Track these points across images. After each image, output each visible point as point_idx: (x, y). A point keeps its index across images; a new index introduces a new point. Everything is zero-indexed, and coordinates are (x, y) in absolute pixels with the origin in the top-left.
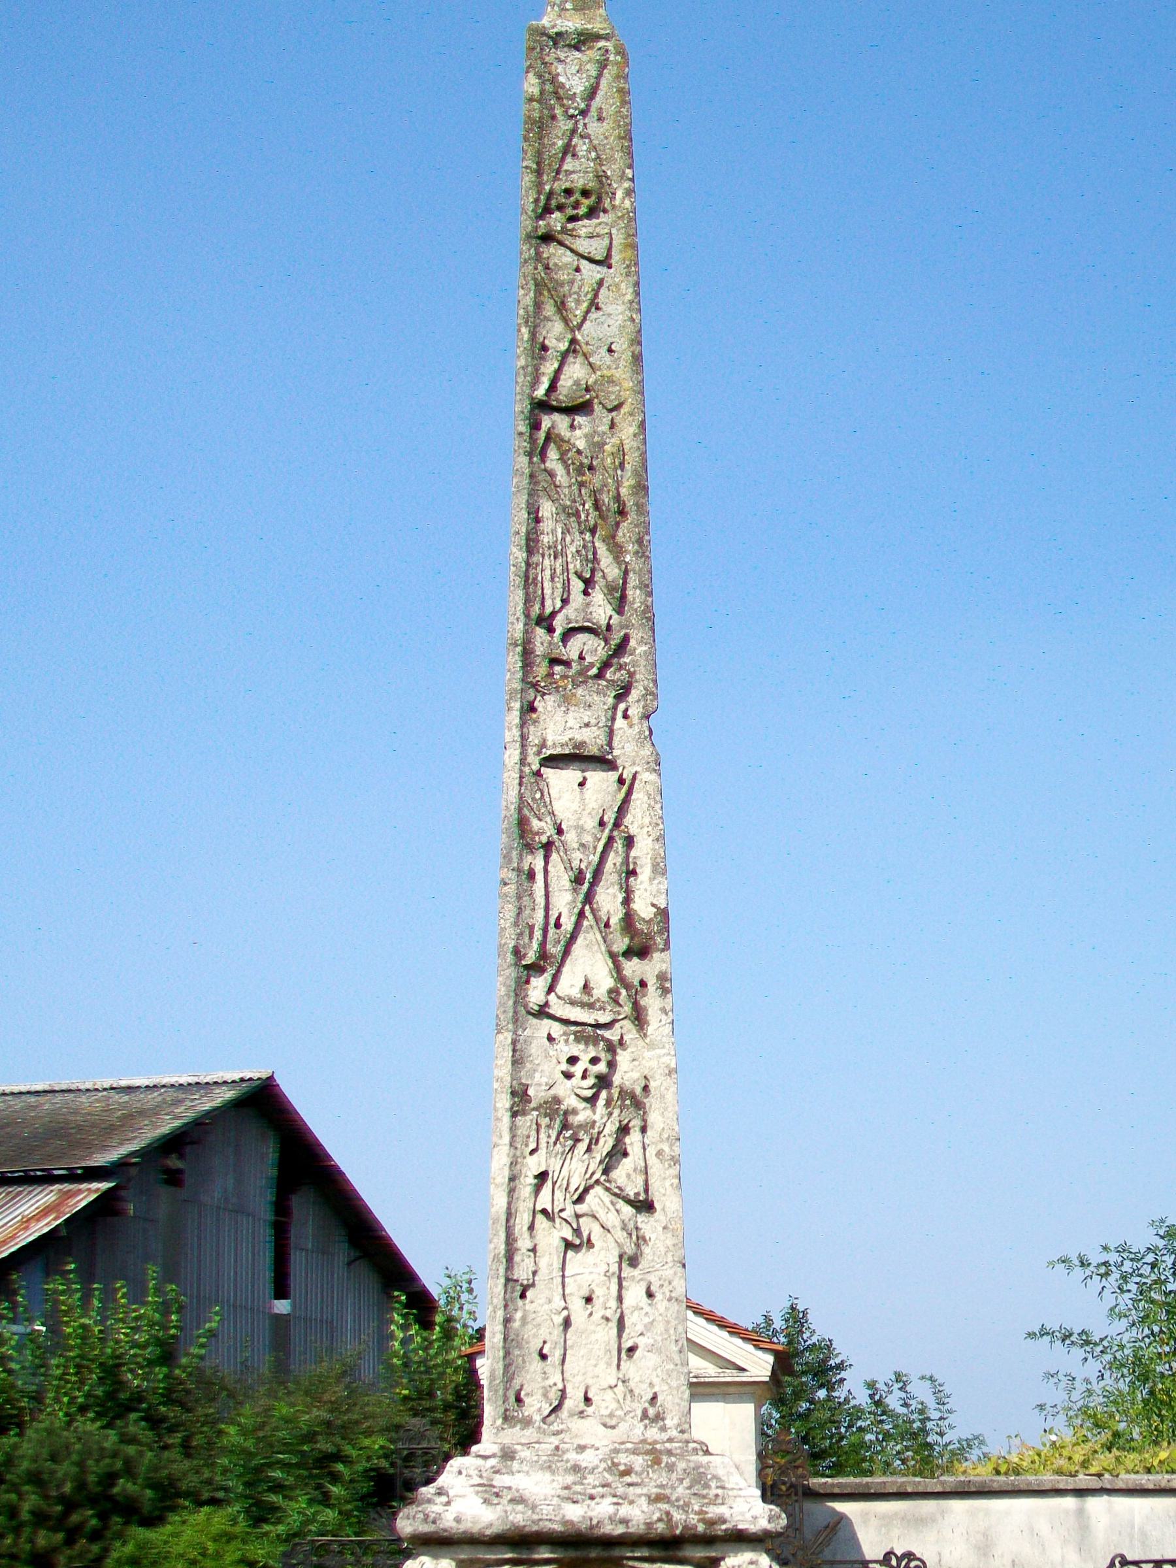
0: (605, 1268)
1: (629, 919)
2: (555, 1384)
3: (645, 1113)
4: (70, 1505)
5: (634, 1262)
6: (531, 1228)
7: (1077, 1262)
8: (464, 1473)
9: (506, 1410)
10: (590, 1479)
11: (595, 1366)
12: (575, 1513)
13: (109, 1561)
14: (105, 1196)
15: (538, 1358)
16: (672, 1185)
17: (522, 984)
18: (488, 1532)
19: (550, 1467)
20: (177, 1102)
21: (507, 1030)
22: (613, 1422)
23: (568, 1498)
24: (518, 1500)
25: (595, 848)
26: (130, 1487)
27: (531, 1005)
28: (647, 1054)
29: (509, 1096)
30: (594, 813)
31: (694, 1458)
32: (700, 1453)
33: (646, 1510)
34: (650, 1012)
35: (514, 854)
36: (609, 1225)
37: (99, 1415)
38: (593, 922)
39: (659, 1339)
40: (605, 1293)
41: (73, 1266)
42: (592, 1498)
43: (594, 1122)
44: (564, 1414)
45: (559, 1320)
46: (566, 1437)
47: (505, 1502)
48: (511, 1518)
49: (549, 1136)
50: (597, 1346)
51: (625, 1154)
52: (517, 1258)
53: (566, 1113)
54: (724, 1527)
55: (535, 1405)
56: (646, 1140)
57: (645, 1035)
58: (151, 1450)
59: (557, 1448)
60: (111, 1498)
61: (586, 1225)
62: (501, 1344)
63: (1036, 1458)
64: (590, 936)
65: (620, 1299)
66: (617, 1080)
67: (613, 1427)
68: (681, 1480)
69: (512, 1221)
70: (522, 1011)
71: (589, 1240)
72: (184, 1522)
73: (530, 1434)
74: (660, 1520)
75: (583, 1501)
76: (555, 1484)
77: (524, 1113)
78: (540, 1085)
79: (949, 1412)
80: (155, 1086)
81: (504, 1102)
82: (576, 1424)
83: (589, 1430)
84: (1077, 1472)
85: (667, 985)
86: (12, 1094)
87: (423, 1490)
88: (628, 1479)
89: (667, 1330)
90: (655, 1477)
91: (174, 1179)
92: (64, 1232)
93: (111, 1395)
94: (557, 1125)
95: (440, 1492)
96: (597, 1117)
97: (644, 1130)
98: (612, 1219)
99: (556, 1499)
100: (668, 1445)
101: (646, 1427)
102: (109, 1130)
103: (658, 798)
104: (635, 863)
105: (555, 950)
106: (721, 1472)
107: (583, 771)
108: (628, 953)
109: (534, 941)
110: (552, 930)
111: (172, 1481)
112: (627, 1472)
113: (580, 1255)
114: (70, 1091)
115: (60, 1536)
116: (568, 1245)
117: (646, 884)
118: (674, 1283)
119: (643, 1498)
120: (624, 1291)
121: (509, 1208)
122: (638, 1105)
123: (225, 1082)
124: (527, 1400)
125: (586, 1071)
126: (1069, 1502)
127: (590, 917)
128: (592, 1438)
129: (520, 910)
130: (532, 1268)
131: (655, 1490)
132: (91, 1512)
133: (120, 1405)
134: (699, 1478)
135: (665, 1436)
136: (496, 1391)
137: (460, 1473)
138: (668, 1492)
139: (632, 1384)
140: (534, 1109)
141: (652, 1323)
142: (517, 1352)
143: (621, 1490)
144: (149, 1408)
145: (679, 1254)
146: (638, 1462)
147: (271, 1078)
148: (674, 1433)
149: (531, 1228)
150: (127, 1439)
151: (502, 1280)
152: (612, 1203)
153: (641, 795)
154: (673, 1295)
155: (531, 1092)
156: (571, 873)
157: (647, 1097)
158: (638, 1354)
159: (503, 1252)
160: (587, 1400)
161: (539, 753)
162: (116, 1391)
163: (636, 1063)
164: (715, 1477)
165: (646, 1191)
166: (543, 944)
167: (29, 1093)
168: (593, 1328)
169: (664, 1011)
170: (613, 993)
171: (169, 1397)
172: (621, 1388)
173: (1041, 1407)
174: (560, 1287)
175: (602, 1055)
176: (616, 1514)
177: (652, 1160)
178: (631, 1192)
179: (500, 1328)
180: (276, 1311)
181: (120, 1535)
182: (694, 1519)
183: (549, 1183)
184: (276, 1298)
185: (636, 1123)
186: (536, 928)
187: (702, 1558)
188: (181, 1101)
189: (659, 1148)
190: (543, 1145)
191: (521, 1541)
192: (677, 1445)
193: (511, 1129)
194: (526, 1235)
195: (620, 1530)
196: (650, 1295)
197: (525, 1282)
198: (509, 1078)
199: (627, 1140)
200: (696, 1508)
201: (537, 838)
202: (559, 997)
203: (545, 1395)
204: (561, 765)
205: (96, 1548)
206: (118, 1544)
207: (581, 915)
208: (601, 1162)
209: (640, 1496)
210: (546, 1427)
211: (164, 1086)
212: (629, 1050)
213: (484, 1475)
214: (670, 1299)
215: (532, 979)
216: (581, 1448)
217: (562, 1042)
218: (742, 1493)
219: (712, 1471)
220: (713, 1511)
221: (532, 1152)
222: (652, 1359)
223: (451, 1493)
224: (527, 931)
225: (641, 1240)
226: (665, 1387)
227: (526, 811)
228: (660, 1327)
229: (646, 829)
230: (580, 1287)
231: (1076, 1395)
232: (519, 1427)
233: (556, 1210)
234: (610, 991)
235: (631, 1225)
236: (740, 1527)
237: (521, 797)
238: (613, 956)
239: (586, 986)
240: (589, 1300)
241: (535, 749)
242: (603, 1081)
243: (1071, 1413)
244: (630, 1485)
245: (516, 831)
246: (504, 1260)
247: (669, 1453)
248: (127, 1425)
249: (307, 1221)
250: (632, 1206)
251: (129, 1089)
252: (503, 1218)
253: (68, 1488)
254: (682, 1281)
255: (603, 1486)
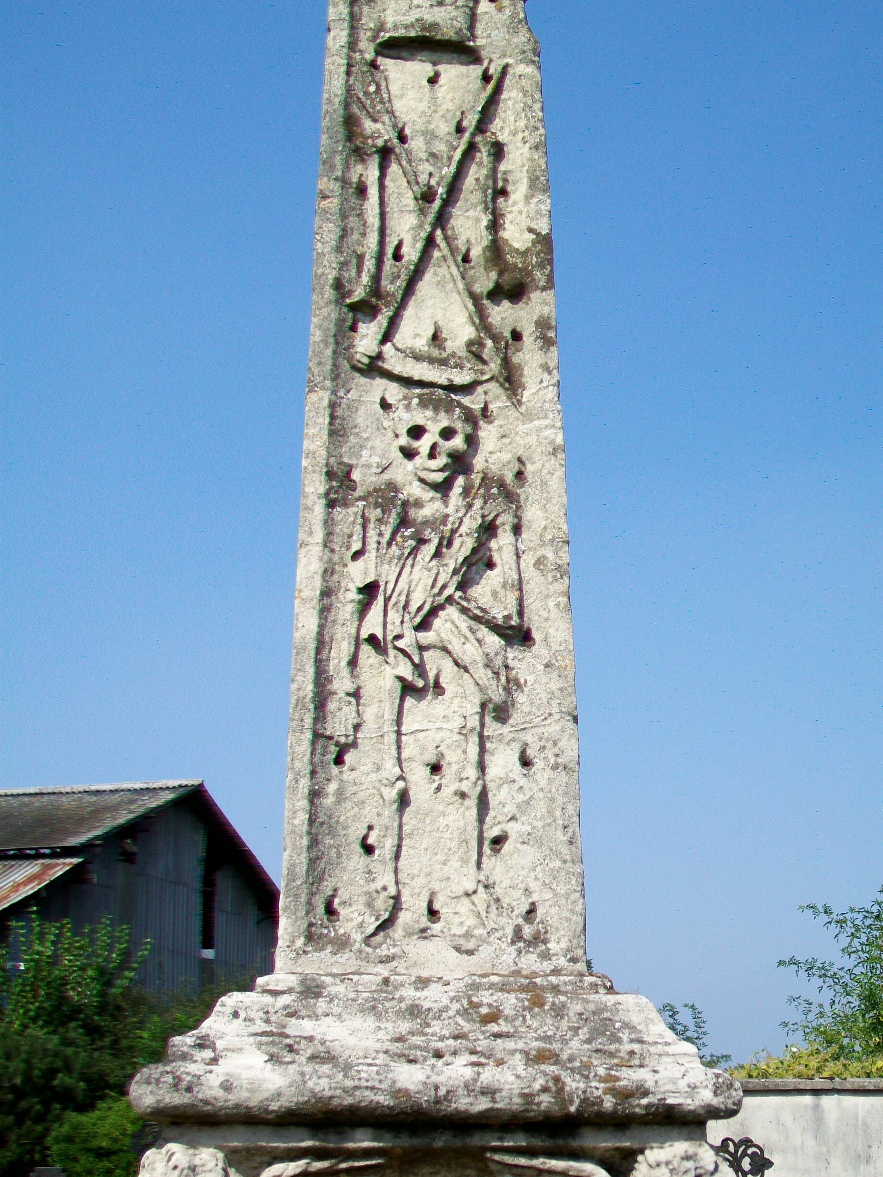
0: (458, 722)
1: (496, 250)
2: (385, 889)
3: (518, 508)
4: (19, 1093)
5: (502, 713)
6: (353, 663)
7: (822, 910)
8: (243, 1015)
9: (311, 925)
10: (436, 1027)
11: (444, 864)
12: (411, 1078)
13: (49, 1138)
14: (76, 867)
15: (361, 851)
16: (557, 605)
17: (345, 331)
18: (274, 1106)
19: (374, 1008)
20: (132, 802)
21: (323, 388)
22: (471, 945)
23: (401, 1056)
24: (325, 1057)
25: (450, 158)
26: (68, 1081)
27: (358, 356)
28: (522, 428)
29: (323, 477)
30: (449, 116)
31: (592, 997)
32: (602, 991)
33: (523, 1074)
34: (526, 372)
35: (338, 160)
36: (466, 660)
37: (47, 1023)
38: (446, 251)
39: (540, 824)
40: (460, 760)
41: (35, 908)
42: (438, 1055)
43: (447, 516)
44: (398, 932)
45: (391, 794)
46: (400, 965)
47: (303, 1059)
48: (310, 1084)
49: (381, 534)
50: (447, 835)
51: (490, 565)
52: (332, 706)
53: (405, 504)
54: (644, 1101)
55: (355, 920)
56: (519, 545)
57: (520, 402)
58: (85, 1051)
59: (386, 981)
60: (52, 1088)
61: (434, 662)
62: (305, 828)
63: (780, 1065)
64: (443, 271)
65: (482, 766)
66: (478, 462)
67: (470, 953)
68: (576, 1030)
69: (324, 656)
70: (346, 366)
71: (437, 685)
72: (110, 1108)
73: (346, 960)
74: (545, 1090)
75: (425, 1059)
76: (381, 1034)
77: (345, 504)
78: (368, 466)
79: (704, 1033)
80: (116, 790)
81: (315, 486)
82: (416, 948)
83: (435, 957)
84: (813, 1075)
85: (551, 334)
86: (12, 795)
87: (177, 1040)
88: (494, 1028)
89: (550, 812)
90: (535, 1024)
91: (129, 858)
92: (44, 894)
93: (57, 1008)
94: (393, 519)
95: (203, 1044)
96: (450, 510)
97: (517, 530)
98: (469, 652)
99: (382, 1056)
100: (553, 979)
101: (520, 952)
102: (81, 820)
103: (537, 96)
104: (506, 181)
105: (392, 287)
106: (635, 1019)
107: (435, 64)
108: (496, 294)
109: (364, 274)
110: (389, 261)
111: (102, 1076)
112: (493, 1017)
113: (424, 704)
114: (54, 793)
115: (11, 1119)
116: (407, 689)
117: (521, 205)
118: (560, 745)
119: (518, 1056)
120: (487, 757)
121: (320, 634)
122: (509, 496)
123: (168, 788)
124: (343, 912)
125: (434, 447)
126: (808, 1099)
127: (443, 244)
128: (438, 966)
129: (344, 234)
130: (353, 720)
131: (536, 1044)
132: (36, 1100)
133: (64, 1016)
134: (603, 1027)
135: (547, 966)
136: (297, 896)
137: (236, 1015)
138: (556, 1046)
139: (499, 891)
140: (360, 499)
141: (528, 803)
142: (328, 841)
143: (483, 1044)
144: (87, 1018)
145: (569, 702)
146: (510, 1002)
147: (201, 785)
148: (562, 962)
149: (353, 663)
150: (67, 1042)
151: (309, 735)
152: (471, 629)
153: (513, 94)
154: (560, 760)
155: (356, 475)
156: (416, 188)
157: (522, 486)
158: (507, 847)
159: (311, 695)
160: (433, 913)
161: (374, 38)
162: (61, 1005)
163: (506, 441)
164: (626, 1025)
165: (521, 613)
166: (376, 278)
167: (25, 795)
168: (441, 808)
169: (547, 369)
170: (475, 350)
171: (102, 1009)
172: (482, 896)
173: (785, 1024)
174: (394, 747)
175: (459, 426)
176: (475, 1080)
177: (530, 572)
178: (498, 614)
179: (304, 803)
180: (204, 956)
181: (59, 1119)
182: (597, 1089)
183: (381, 599)
184: (205, 948)
185: (506, 520)
186: (367, 257)
187: (607, 1150)
188: (136, 801)
189: (539, 554)
190: (372, 545)
191: (322, 1122)
192: (566, 979)
193: (326, 522)
194: (345, 672)
195: (482, 1105)
196: (526, 763)
197: (343, 740)
198: (324, 453)
199: (493, 544)
200: (601, 1071)
201: (370, 141)
202: (398, 349)
203: (369, 905)
204: (404, 54)
205: (39, 1128)
206: (56, 1125)
207: (430, 242)
208: (455, 572)
209: (513, 1052)
210: (370, 950)
211: (122, 790)
212: (497, 423)
213: (273, 1018)
214: (555, 767)
215: (360, 324)
216: (423, 983)
217: (401, 407)
218: (670, 1049)
219: (622, 1016)
220: (629, 1077)
221: (357, 555)
222: (530, 854)
223: (220, 1045)
224: (354, 261)
225: (513, 685)
226: (549, 895)
227: (355, 109)
228: (540, 808)
229: (520, 136)
230: (423, 749)
231: (811, 1017)
232: (329, 949)
233: (390, 638)
234: (470, 344)
235: (498, 662)
236: (669, 1101)
237: (349, 90)
238: (475, 298)
239: (436, 338)
240: (436, 768)
241: (369, 34)
242: (460, 463)
243: (807, 1030)
244: (497, 1036)
245: (341, 133)
246: (312, 706)
247: (555, 989)
248: (67, 1031)
249: (227, 891)
250: (501, 635)
251: (98, 792)
252: (312, 646)
253: (18, 1081)
254: (574, 740)
255: (456, 1038)
